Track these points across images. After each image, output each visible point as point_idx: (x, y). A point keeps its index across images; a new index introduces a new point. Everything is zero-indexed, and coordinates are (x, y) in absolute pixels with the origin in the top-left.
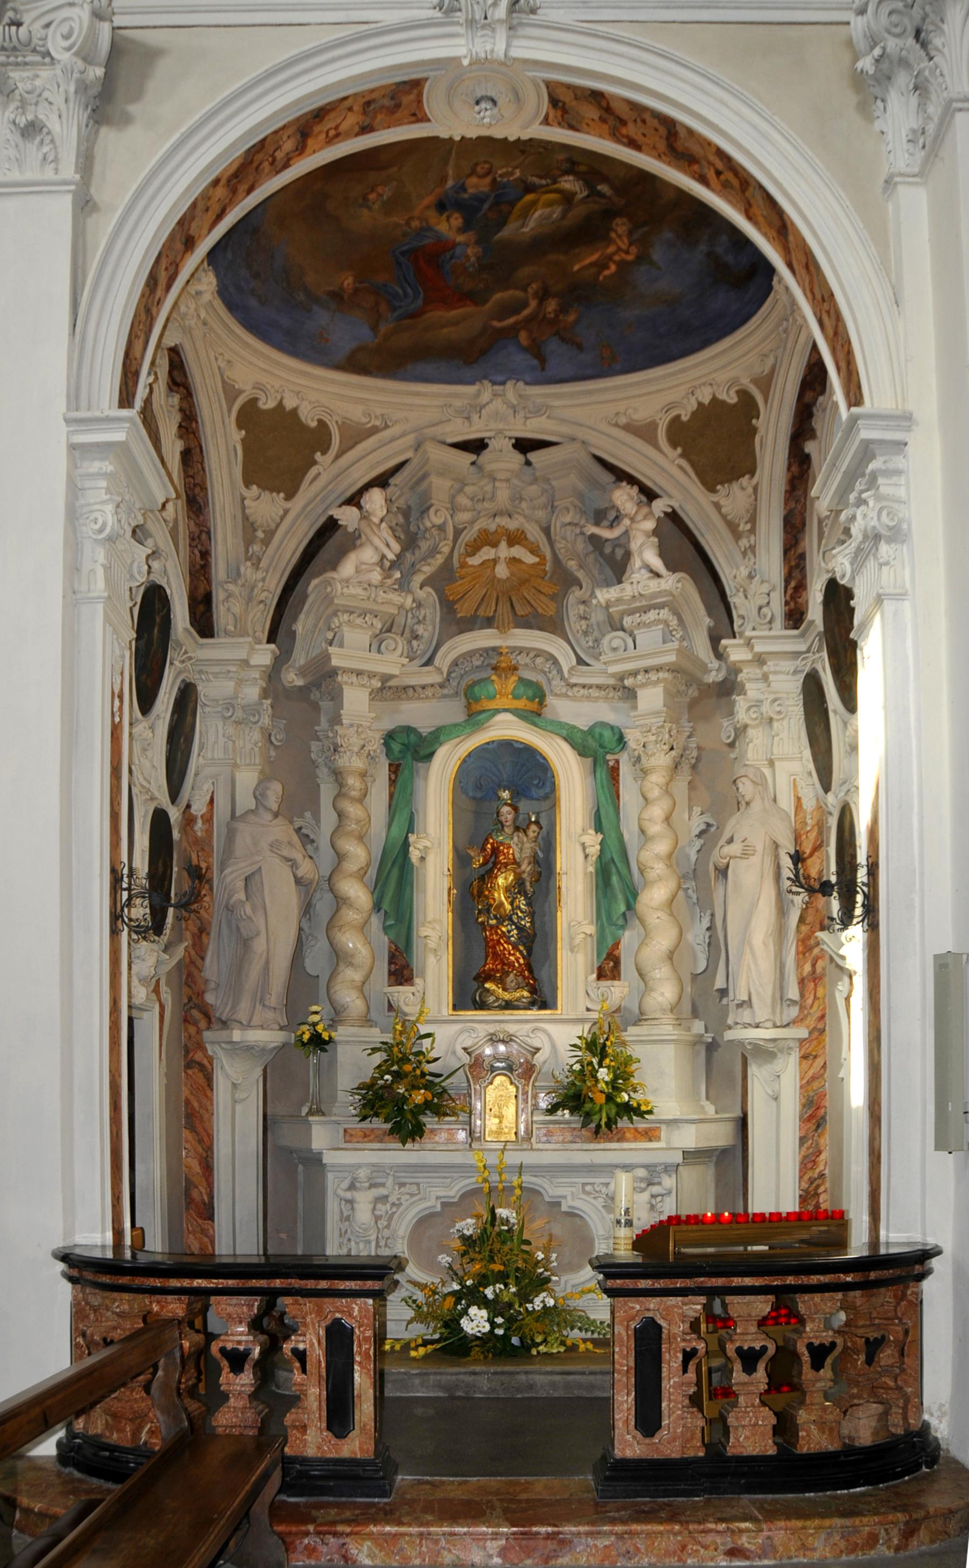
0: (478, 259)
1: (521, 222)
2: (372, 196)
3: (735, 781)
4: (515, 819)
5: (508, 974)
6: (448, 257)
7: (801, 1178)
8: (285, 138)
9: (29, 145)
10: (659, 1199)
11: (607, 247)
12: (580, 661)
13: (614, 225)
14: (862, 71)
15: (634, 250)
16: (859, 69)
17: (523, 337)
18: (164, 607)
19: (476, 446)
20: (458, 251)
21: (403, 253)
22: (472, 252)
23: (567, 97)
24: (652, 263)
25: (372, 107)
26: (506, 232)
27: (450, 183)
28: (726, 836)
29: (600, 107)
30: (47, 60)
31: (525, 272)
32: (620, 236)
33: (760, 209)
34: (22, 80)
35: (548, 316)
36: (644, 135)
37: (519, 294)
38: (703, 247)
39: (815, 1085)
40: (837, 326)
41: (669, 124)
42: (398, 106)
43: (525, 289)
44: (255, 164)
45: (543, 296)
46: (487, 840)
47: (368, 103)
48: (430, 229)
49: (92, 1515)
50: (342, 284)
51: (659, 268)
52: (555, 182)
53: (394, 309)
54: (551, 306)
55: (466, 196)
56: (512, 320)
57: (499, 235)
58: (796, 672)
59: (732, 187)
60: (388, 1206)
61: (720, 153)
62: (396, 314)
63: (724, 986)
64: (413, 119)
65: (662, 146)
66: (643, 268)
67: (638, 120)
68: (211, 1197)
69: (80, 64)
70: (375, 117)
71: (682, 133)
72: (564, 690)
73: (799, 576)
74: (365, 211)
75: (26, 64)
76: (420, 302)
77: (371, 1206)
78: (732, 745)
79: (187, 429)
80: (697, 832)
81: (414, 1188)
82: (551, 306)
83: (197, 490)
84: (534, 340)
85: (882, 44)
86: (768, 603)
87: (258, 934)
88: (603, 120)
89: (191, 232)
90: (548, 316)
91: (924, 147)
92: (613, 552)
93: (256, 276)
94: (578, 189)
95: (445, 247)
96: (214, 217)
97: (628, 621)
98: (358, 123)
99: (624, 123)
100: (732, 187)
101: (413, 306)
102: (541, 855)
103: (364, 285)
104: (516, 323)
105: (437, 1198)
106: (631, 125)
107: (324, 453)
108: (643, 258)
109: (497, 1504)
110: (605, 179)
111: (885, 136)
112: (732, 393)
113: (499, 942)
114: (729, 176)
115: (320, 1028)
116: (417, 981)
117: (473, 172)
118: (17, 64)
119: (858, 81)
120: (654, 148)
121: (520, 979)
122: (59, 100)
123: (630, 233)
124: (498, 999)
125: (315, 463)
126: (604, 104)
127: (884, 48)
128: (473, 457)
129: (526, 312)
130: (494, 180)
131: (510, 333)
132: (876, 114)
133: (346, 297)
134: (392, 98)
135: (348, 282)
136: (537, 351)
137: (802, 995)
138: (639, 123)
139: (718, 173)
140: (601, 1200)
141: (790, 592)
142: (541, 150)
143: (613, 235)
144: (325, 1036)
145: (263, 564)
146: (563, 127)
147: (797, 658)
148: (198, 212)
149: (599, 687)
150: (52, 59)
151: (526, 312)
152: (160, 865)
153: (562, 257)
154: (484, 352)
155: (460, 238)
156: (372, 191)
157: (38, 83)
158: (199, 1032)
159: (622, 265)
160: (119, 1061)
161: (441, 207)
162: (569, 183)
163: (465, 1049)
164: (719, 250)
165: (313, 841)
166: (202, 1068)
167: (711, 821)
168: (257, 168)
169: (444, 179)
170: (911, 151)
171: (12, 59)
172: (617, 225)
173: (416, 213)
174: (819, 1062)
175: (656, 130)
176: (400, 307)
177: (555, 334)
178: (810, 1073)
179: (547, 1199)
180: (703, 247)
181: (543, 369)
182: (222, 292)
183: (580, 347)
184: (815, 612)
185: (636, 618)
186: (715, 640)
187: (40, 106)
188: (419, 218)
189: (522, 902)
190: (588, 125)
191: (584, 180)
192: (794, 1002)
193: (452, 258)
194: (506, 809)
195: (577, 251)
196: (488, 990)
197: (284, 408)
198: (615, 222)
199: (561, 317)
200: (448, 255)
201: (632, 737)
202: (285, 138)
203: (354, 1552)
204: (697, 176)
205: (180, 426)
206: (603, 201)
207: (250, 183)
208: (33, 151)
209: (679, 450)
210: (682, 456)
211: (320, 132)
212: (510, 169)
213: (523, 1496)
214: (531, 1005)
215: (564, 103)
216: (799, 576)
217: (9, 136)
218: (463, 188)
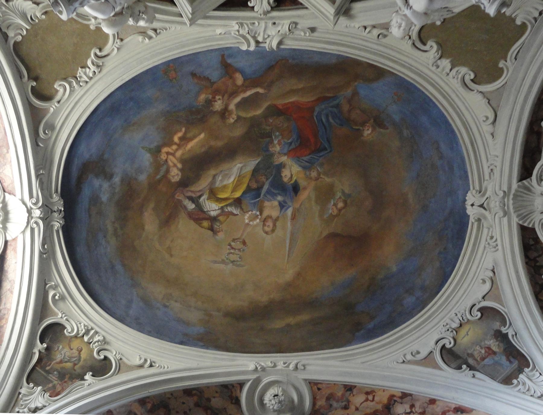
0: (272, 142)
1: (243, 172)
6: (293, 144)
13: (180, 174)
15: (163, 157)
20: (285, 151)
21: (325, 149)
24: (150, 150)
25: (344, 404)
26: (252, 163)
27: (289, 212)
31: (238, 132)
32: (175, 165)
35: (220, 97)
36: (183, 403)
37: (243, 114)
38: (117, 179)
43: (239, 118)
45: (224, 113)
48: (304, 168)
50: (372, 131)
51: (143, 148)
52: (222, 208)
53: (338, 106)
54: (218, 105)
55: (280, 198)
57: (257, 162)
62: (335, 102)
64: (319, 386)
66: (155, 144)
70: (343, 395)
74: (347, 191)
76: (317, 109)
82: (218, 105)
84: (231, 77)
90: (220, 97)
92: (158, 165)
99: (197, 405)
101: (323, 107)
103: (357, 128)
104: (245, 91)
106: (192, 405)
108: (156, 152)
120: (176, 398)
123: (168, 171)
129: (238, 99)
130: (261, 214)
133: (372, 121)
134: (331, 406)
135: (367, 132)
143: (180, 166)
151: (238, 99)
153: (213, 143)
154: (271, 68)
156: (340, 210)
159: (170, 143)
161: (296, 189)
164: (106, 185)
169: (293, 218)
172: (178, 175)
173: (313, 183)
176: (332, 107)
177: (214, 83)
180: (117, 179)
183: (193, 75)
188: (311, 178)
190: (217, 392)
193: (291, 144)
195: (203, 150)
197: (451, 62)
198: (180, 177)
199: (210, 97)
200: (293, 146)
204: (148, 400)
206: (189, 194)
212: (251, 223)
215: (232, 403)
218: (282, 206)
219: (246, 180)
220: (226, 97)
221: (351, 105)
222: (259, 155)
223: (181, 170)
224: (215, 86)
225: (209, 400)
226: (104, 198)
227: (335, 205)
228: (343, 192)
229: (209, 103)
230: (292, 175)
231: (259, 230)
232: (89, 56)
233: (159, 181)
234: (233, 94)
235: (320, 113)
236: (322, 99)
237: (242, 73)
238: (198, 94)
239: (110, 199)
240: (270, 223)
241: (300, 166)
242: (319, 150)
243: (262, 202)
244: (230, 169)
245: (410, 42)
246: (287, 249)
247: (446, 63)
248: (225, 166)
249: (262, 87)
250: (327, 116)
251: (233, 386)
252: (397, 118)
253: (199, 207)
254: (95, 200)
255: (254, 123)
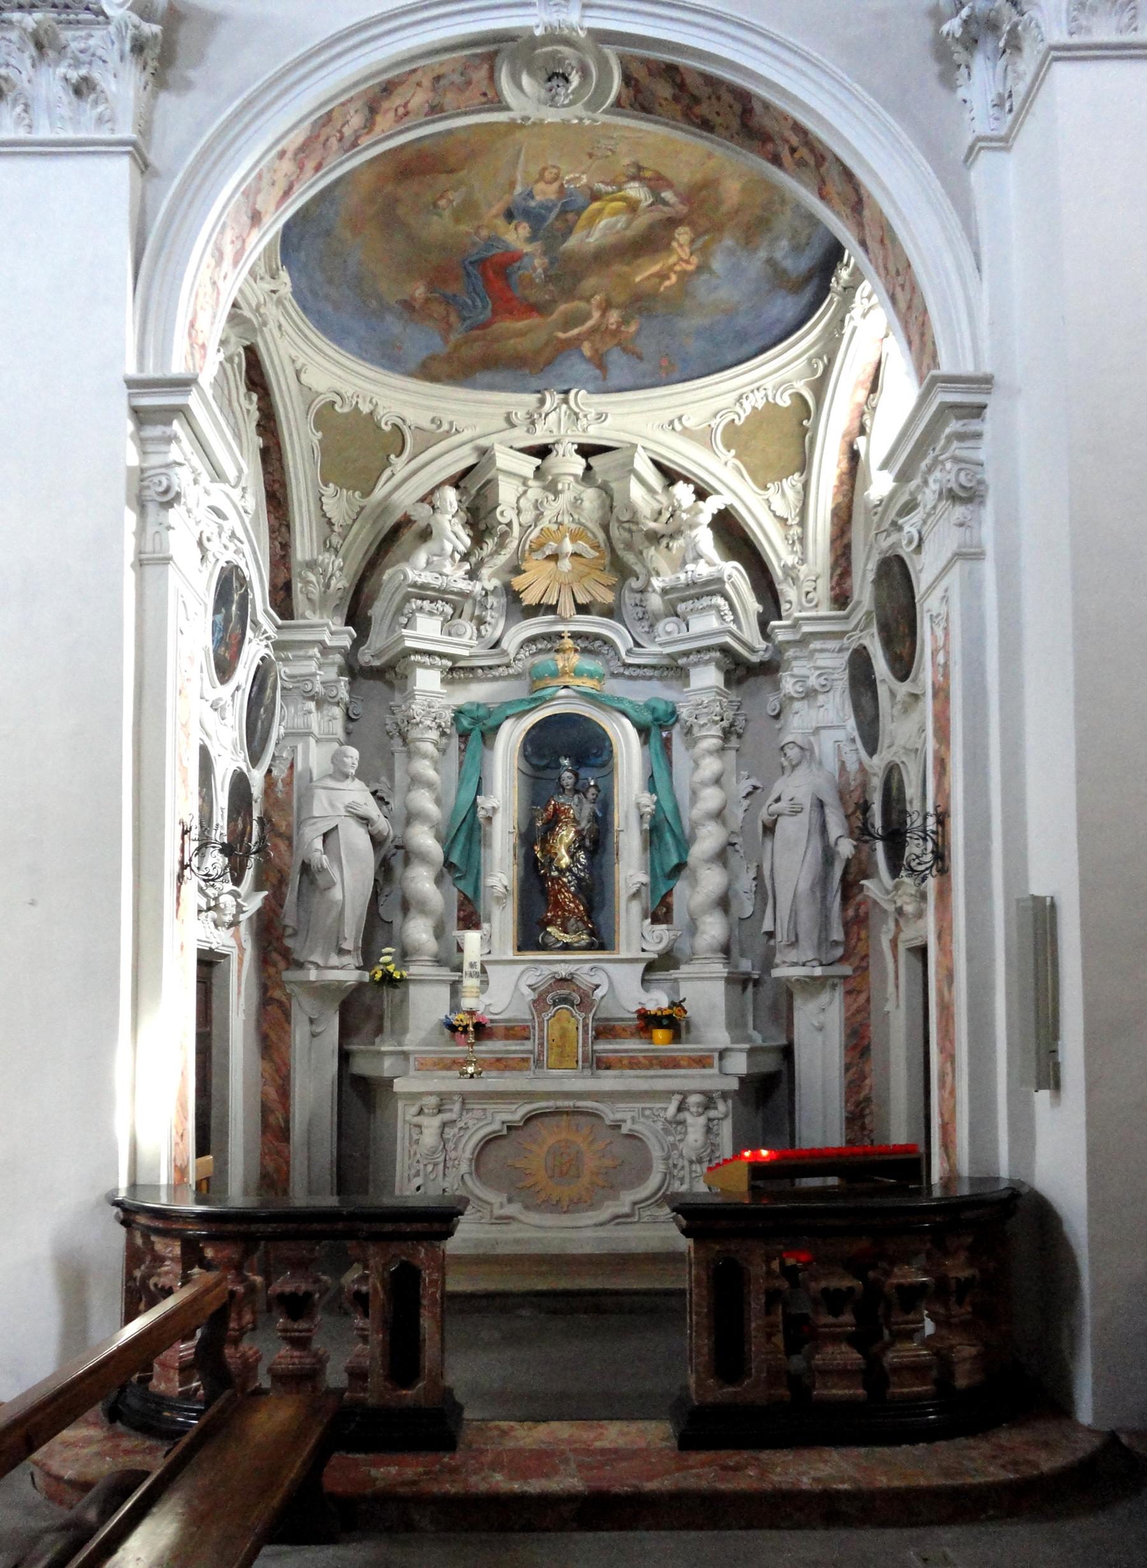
0: (545, 270)
1: (585, 232)
2: (442, 203)
3: (782, 748)
4: (576, 783)
5: (569, 919)
7: (847, 1101)
8: (352, 112)
9: (82, 104)
10: (716, 1122)
11: (669, 256)
12: (637, 644)
14: (948, 34)
15: (695, 260)
16: (945, 33)
17: (587, 349)
18: (242, 586)
19: (542, 452)
20: (526, 260)
21: (471, 263)
22: (539, 263)
23: (640, 73)
24: (711, 272)
26: (572, 242)
27: (519, 189)
28: (774, 796)
29: (674, 84)
30: (101, 18)
31: (590, 283)
32: (681, 246)
33: (835, 184)
34: (75, 39)
36: (718, 114)
37: (582, 304)
38: (762, 254)
39: (859, 1018)
40: (911, 300)
41: (743, 98)
42: (469, 83)
43: (588, 300)
44: (322, 139)
45: (607, 306)
46: (549, 801)
47: (438, 78)
48: (498, 239)
49: (98, 1540)
52: (620, 190)
53: (464, 319)
54: (614, 317)
55: (533, 204)
56: (575, 331)
58: (841, 650)
59: (806, 165)
60: (456, 1130)
61: (798, 128)
63: (772, 929)
65: (735, 123)
67: (713, 97)
68: (287, 1121)
69: (135, 19)
71: (758, 107)
72: (621, 670)
73: (844, 564)
74: (435, 218)
75: (78, 22)
76: (488, 313)
77: (439, 1131)
78: (777, 717)
79: (264, 427)
80: (744, 794)
81: (480, 1113)
82: (614, 317)
83: (276, 486)
84: (596, 351)
85: (970, 4)
86: (815, 589)
87: (334, 884)
88: (676, 99)
89: (258, 207)
91: (1010, 111)
93: (330, 281)
94: (643, 196)
95: (515, 257)
96: (281, 193)
97: (681, 608)
98: (427, 102)
99: (696, 100)
100: (806, 165)
101: (482, 317)
102: (600, 814)
105: (503, 1123)
107: (399, 454)
109: (571, 1455)
110: (670, 185)
111: (968, 104)
112: (786, 396)
113: (560, 892)
114: (803, 152)
115: (391, 968)
116: (485, 926)
117: (541, 177)
118: (70, 22)
119: (941, 50)
121: (580, 924)
122: (113, 57)
123: (692, 241)
124: (558, 941)
125: (390, 464)
126: (678, 80)
127: (972, 8)
128: (538, 461)
129: (590, 324)
130: (562, 185)
131: (573, 345)
132: (958, 83)
134: (462, 74)
135: (420, 291)
136: (600, 362)
137: (847, 934)
138: (714, 100)
139: (793, 150)
140: (660, 1124)
141: (835, 578)
142: (610, 153)
143: (675, 244)
144: (397, 975)
145: (341, 553)
146: (636, 110)
147: (842, 638)
148: (265, 183)
149: (653, 667)
150: (107, 18)
151: (590, 324)
152: (240, 821)
153: (626, 269)
154: (549, 362)
155: (527, 248)
156: (442, 197)
157: (92, 42)
158: (278, 972)
159: (683, 275)
160: (1004, 731)
161: (509, 215)
162: (635, 191)
163: (529, 986)
164: (778, 255)
165: (387, 803)
166: (281, 1004)
167: (758, 784)
168: (324, 144)
169: (512, 185)
170: (996, 115)
171: (64, 16)
174: (862, 998)
175: (731, 107)
178: (855, 1006)
179: (608, 1123)
180: (762, 254)
181: (605, 379)
182: (297, 293)
183: (640, 358)
184: (863, 590)
185: (689, 604)
186: (763, 624)
187: (94, 66)
188: (487, 227)
189: (582, 856)
191: (650, 187)
192: (836, 943)
193: (519, 268)
194: (568, 774)
196: (550, 933)
197: (361, 412)
198: (677, 231)
200: (517, 264)
201: (684, 713)
202: (352, 112)
203: (417, 1517)
205: (258, 425)
206: (666, 209)
207: (317, 161)
208: (90, 111)
209: (733, 452)
210: (735, 457)
211: (387, 111)
213: (598, 1444)
214: (590, 947)
216: (844, 564)
217: (62, 94)
218: (531, 195)
219: (582, 222)
220: (603, 328)
221: (447, 323)
222: (563, 253)
223: (673, 239)
224: (616, 341)
225: (676, 99)
226: (784, 243)
227: (451, 201)
228: (440, 216)
229: (625, 321)
230: (516, 229)
231: (564, 167)
232: (747, 418)
233: (706, 232)
234: (593, 331)
235: (484, 307)
236: (485, 325)
237: (582, 356)
238: (638, 333)
239: (777, 238)
240: (548, 175)
241: (504, 241)
242: (481, 263)
243: (559, 199)
244: (604, 235)
245: (408, 423)
246: (522, 157)
247: (365, 408)
248: (612, 239)
249: (558, 339)
250: (475, 306)
251: (631, 106)
252: (389, 318)
253: (655, 192)
254: (797, 249)
255: (569, 294)
